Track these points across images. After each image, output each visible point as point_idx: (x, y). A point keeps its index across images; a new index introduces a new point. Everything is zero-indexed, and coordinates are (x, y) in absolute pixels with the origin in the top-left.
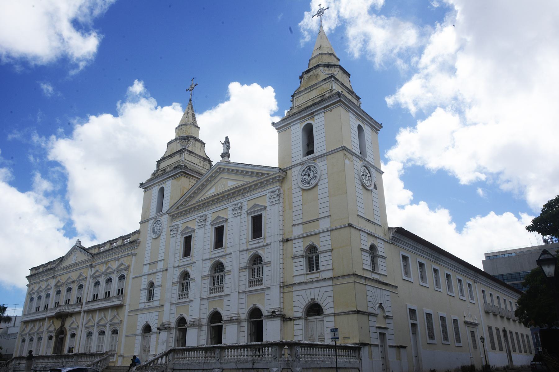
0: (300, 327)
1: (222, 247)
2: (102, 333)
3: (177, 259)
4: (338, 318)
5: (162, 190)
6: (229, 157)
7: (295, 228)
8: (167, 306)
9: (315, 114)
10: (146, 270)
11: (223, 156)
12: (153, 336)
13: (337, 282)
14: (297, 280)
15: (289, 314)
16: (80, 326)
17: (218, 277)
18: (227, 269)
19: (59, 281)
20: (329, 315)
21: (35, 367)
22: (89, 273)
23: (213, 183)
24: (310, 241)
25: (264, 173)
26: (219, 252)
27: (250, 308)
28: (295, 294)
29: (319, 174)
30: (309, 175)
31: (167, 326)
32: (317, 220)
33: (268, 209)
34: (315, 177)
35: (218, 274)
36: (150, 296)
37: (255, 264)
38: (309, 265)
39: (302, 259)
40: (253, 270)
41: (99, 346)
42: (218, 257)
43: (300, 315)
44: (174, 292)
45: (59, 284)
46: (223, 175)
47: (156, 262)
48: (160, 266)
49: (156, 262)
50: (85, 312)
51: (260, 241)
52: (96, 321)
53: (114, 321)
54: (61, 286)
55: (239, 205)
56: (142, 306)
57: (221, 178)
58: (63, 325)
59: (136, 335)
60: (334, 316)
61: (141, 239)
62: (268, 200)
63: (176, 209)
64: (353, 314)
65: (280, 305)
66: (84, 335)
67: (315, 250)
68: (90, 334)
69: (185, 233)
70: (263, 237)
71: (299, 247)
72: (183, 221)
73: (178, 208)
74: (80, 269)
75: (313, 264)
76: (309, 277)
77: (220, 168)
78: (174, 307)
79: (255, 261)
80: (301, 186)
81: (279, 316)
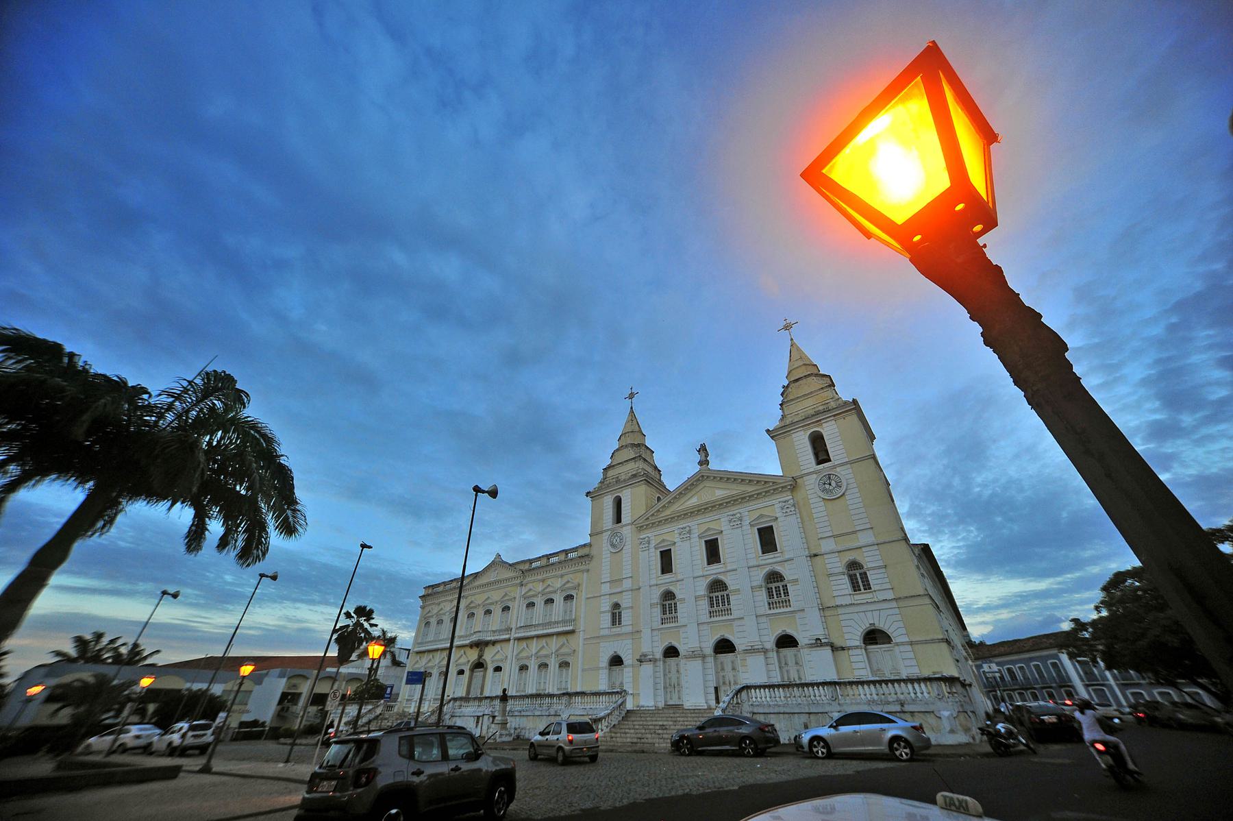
0: (860, 658)
1: (672, 572)
2: (544, 666)
3: (654, 576)
4: (916, 647)
5: (618, 503)
6: (708, 465)
7: (823, 542)
8: (646, 633)
9: (792, 432)
10: (606, 589)
11: (701, 463)
12: (626, 670)
13: (901, 604)
14: (839, 601)
15: (838, 643)
16: (509, 657)
17: (723, 596)
18: (731, 588)
19: (472, 602)
20: (629, 666)
21: (491, 711)
22: (518, 592)
23: (693, 492)
24: (615, 599)
25: (760, 481)
26: (715, 568)
27: (775, 635)
28: (841, 617)
29: (844, 484)
30: (830, 484)
31: (651, 656)
32: (854, 532)
33: (724, 533)
34: (839, 486)
35: (717, 594)
36: (616, 618)
37: (666, 600)
38: (853, 583)
39: (843, 577)
40: (711, 598)
41: (540, 683)
42: (716, 574)
43: (858, 643)
44: (655, 614)
45: (472, 605)
46: (707, 483)
47: (621, 580)
48: (627, 584)
49: (621, 580)
50: (516, 639)
51: (776, 555)
52: (534, 652)
53: (562, 651)
54: (475, 607)
55: (739, 515)
56: (603, 633)
57: (705, 486)
58: (480, 656)
59: (598, 668)
60: (911, 645)
61: (594, 552)
62: (677, 535)
63: (646, 519)
64: (939, 642)
65: (824, 631)
66: (516, 669)
67: (671, 596)
68: (523, 668)
69: (661, 547)
70: (779, 551)
71: (837, 564)
72: (656, 533)
73: (648, 518)
74: (507, 586)
75: (858, 582)
76: (857, 597)
77: (703, 476)
78: (655, 633)
79: (666, 597)
80: (820, 495)
81: (826, 644)
